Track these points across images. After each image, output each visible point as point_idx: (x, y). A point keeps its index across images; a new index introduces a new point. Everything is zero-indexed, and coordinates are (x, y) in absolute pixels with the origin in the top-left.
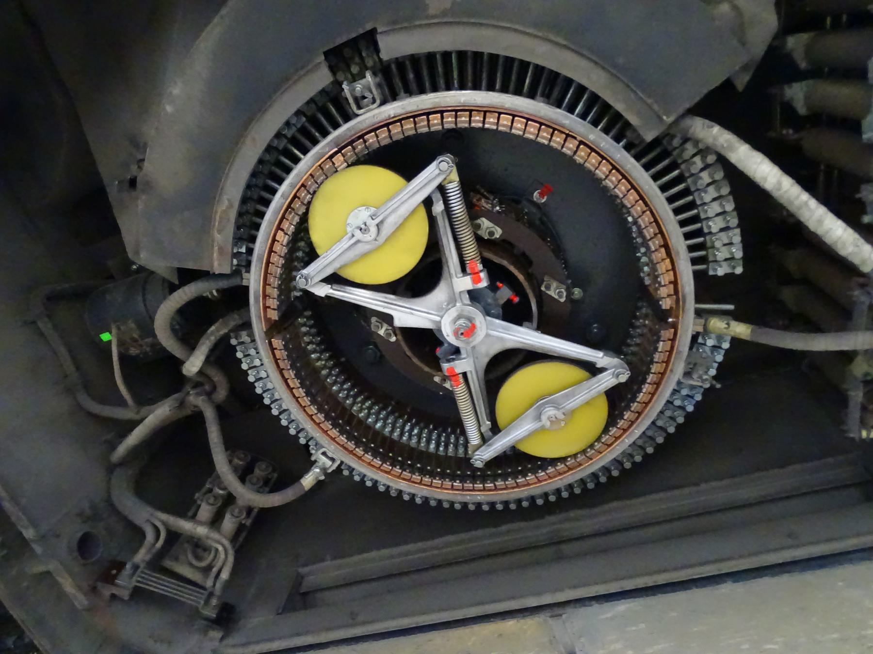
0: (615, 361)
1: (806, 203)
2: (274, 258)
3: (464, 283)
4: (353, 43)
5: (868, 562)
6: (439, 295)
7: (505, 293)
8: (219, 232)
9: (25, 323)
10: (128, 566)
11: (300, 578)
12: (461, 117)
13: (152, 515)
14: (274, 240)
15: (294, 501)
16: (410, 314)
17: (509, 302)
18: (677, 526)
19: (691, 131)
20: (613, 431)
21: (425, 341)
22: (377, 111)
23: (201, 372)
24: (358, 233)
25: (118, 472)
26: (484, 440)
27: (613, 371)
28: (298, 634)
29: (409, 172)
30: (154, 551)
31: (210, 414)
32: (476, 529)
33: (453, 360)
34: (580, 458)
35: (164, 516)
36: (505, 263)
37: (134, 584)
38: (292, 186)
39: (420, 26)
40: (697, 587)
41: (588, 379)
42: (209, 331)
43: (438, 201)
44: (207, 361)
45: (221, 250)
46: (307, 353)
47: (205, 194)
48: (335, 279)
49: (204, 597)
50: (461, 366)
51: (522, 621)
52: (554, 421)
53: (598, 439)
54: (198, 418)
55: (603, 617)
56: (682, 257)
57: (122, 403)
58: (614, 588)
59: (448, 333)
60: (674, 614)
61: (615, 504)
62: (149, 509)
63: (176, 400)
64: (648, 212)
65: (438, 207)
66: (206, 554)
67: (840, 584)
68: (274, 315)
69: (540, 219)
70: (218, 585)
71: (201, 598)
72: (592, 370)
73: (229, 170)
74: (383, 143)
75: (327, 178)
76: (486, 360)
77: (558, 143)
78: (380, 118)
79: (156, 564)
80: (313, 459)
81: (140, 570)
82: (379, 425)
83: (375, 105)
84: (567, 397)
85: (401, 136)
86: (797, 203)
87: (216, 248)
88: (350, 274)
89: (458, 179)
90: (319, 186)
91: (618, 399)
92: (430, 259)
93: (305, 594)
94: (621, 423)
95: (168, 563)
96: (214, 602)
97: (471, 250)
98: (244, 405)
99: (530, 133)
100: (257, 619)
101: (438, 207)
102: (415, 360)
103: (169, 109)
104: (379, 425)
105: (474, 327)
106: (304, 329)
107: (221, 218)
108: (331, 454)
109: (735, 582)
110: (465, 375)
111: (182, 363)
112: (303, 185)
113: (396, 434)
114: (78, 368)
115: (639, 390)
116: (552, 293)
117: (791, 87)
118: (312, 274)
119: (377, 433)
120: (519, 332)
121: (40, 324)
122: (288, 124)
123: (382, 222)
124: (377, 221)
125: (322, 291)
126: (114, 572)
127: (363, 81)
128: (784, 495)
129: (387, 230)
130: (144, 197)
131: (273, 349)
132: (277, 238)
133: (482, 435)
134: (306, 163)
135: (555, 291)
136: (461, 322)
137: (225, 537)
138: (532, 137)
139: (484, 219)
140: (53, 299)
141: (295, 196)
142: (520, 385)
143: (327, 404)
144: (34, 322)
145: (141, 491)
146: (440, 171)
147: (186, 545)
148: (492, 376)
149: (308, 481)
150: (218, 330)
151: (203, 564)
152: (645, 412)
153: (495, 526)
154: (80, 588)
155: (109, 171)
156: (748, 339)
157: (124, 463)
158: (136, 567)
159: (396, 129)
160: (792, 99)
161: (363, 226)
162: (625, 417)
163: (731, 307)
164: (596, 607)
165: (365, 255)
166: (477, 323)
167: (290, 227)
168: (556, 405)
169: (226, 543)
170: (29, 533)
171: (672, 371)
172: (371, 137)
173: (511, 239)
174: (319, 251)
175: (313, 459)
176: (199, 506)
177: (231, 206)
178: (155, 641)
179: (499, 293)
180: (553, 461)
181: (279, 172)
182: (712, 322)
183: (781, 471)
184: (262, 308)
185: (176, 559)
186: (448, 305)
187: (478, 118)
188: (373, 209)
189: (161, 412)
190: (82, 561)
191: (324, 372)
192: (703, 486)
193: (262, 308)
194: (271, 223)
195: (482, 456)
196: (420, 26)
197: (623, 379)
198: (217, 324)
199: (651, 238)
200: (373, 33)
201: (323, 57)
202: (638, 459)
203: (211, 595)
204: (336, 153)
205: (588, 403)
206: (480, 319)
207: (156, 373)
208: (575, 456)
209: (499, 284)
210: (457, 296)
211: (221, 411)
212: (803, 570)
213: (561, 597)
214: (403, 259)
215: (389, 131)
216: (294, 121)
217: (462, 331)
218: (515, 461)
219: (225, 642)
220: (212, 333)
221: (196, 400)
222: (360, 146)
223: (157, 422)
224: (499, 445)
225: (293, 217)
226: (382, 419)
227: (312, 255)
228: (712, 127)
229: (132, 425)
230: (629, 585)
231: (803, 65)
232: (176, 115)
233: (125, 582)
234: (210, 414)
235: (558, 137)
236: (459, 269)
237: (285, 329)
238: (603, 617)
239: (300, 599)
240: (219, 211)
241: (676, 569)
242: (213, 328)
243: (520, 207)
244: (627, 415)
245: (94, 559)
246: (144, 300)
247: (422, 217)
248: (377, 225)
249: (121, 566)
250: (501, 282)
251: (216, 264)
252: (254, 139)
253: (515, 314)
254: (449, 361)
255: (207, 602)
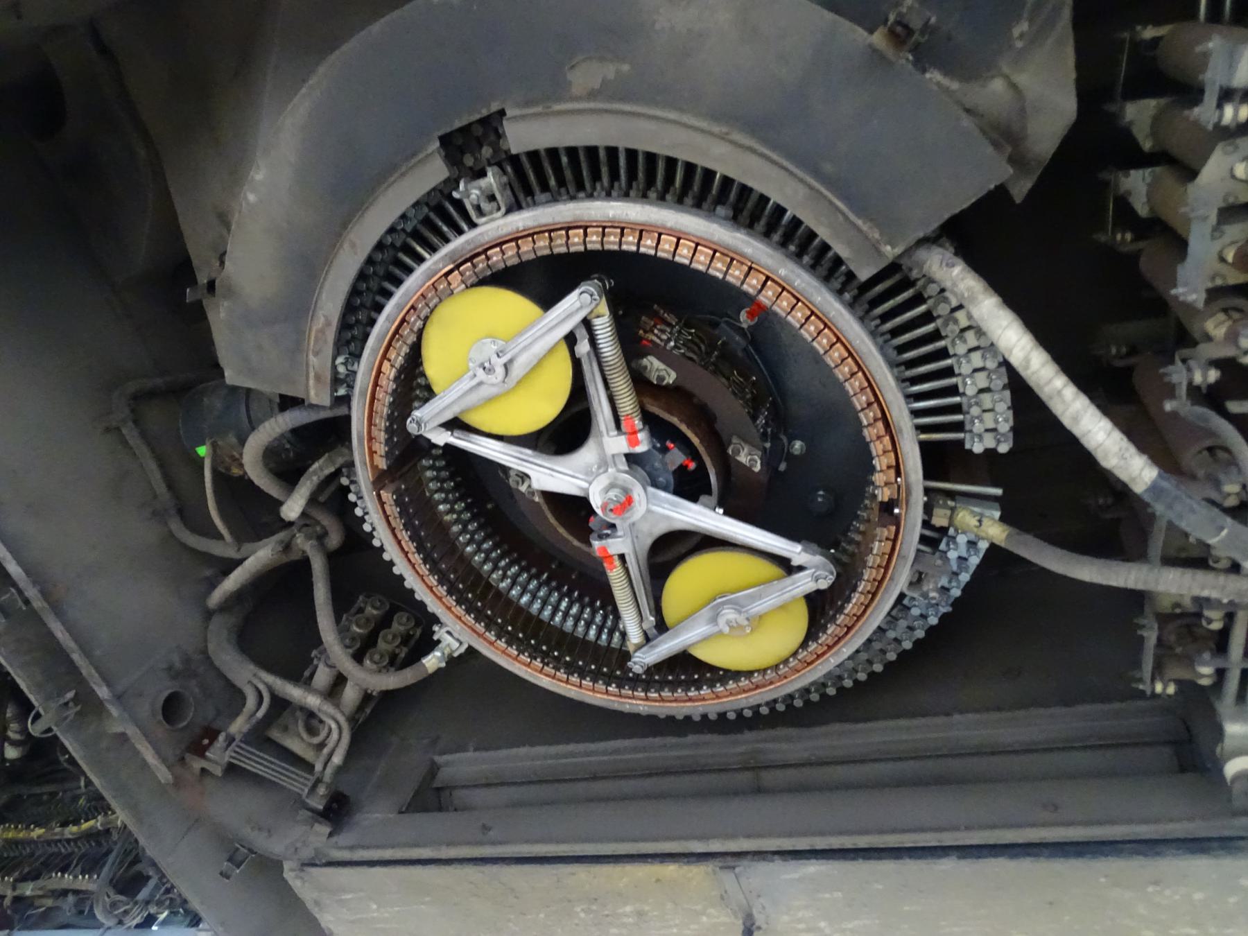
0: (818, 559)
1: (1059, 392)
2: (380, 394)
3: (617, 444)
4: (484, 121)
5: (1141, 857)
6: (586, 455)
7: (677, 457)
8: (316, 354)
9: (108, 430)
10: (221, 738)
11: (434, 769)
12: (610, 234)
13: (255, 675)
14: (379, 372)
15: (413, 685)
16: (550, 475)
17: (682, 469)
18: (909, 767)
19: (926, 267)
20: (813, 646)
21: (574, 510)
22: (501, 222)
23: (304, 514)
24: (480, 372)
25: (217, 621)
26: (647, 639)
27: (815, 571)
28: (417, 845)
29: (547, 301)
30: (254, 721)
31: (318, 566)
32: (655, 736)
33: (608, 536)
34: (770, 675)
35: (270, 679)
36: (675, 420)
37: (227, 759)
38: (399, 307)
39: (560, 113)
40: (910, 857)
41: (778, 579)
42: (311, 469)
43: (583, 338)
44: (313, 500)
45: (318, 378)
46: (431, 505)
47: (297, 308)
48: (455, 424)
49: (310, 784)
50: (616, 546)
51: (686, 868)
52: (735, 627)
53: (795, 654)
54: (305, 563)
55: (788, 877)
56: (905, 436)
57: (219, 537)
58: (802, 844)
59: (596, 502)
60: (880, 887)
61: (837, 727)
62: (252, 667)
63: (281, 542)
64: (860, 374)
65: (583, 347)
66: (321, 726)
67: (1103, 880)
68: (382, 464)
69: (745, 350)
70: (329, 771)
71: (305, 785)
72: (787, 566)
73: (325, 279)
74: (509, 263)
75: (441, 301)
76: (649, 542)
77: (737, 278)
78: (505, 231)
79: (259, 737)
80: (435, 638)
81: (234, 744)
82: (525, 599)
83: (499, 214)
84: (753, 598)
85: (532, 256)
86: (1047, 389)
87: (312, 375)
88: (473, 419)
89: (608, 313)
90: (432, 312)
91: (820, 607)
92: (575, 409)
93: (438, 789)
94: (823, 638)
95: (275, 734)
96: (322, 790)
97: (627, 404)
98: (356, 563)
99: (699, 262)
100: (375, 815)
101: (583, 347)
102: (561, 530)
103: (252, 197)
104: (525, 599)
105: (629, 501)
106: (429, 474)
107: (316, 337)
108: (456, 633)
109: (959, 858)
110: (622, 557)
111: (281, 503)
112: (413, 307)
113: (547, 613)
114: (170, 487)
115: (848, 600)
116: (743, 458)
117: (1127, 176)
118: (426, 418)
119: (520, 611)
120: (690, 510)
121: (124, 431)
122: (404, 217)
123: (511, 361)
124: (505, 359)
125: (441, 438)
126: (206, 741)
127: (483, 182)
128: (1060, 746)
129: (518, 370)
130: (226, 304)
131: (382, 504)
132: (383, 369)
133: (645, 634)
134: (413, 283)
135: (748, 457)
136: (612, 494)
137: (343, 713)
138: (701, 268)
139: (651, 358)
140: (139, 398)
141: (403, 321)
142: (690, 580)
143: (455, 572)
144: (118, 429)
145: (245, 643)
146: (583, 302)
147: (298, 713)
148: (660, 559)
149: (432, 662)
150: (321, 469)
151: (316, 740)
152: (856, 628)
153: (679, 736)
154: (164, 760)
155: (198, 251)
156: (1003, 545)
157: (225, 607)
158: (230, 740)
159: (526, 246)
160: (1129, 193)
161: (487, 365)
162: (829, 632)
163: (998, 492)
164: (777, 865)
165: (490, 400)
166: (635, 497)
167: (398, 356)
168: (738, 606)
169: (342, 719)
170: (103, 692)
171: (891, 579)
172: (496, 254)
173: (688, 386)
174: (435, 389)
175: (435, 638)
176: (316, 667)
177: (328, 324)
178: (252, 828)
179: (669, 457)
180: (736, 675)
181: (397, 272)
182: (961, 515)
183: (1064, 710)
184: (367, 451)
185: (285, 729)
186: (599, 468)
187: (631, 239)
188: (501, 343)
189: (261, 556)
190: (167, 726)
191: (455, 529)
192: (957, 717)
193: (367, 451)
194: (375, 351)
195: (643, 659)
196: (560, 113)
197: (824, 585)
198: (321, 461)
199: (863, 409)
200: (502, 113)
201: (438, 144)
202: (862, 676)
203: (319, 781)
204: (451, 272)
205: (783, 607)
206: (638, 492)
207: (252, 512)
208: (763, 671)
209: (669, 444)
210: (610, 460)
211: (333, 558)
212: (1052, 856)
213: (733, 846)
214: (543, 405)
215: (518, 247)
216: (412, 213)
217: (612, 506)
218: (685, 669)
219: (335, 839)
220: (315, 473)
221: (304, 544)
222: (481, 263)
223: (259, 567)
224: (666, 647)
225: (401, 347)
226: (531, 592)
227: (429, 393)
228: (953, 266)
229: (228, 566)
230: (820, 843)
231: (1147, 145)
232: (266, 203)
233: (218, 755)
234: (318, 566)
235: (737, 268)
236: (612, 424)
237: (401, 476)
238: (788, 877)
239: (431, 797)
240: (314, 329)
241: (882, 832)
242: (316, 465)
243: (717, 332)
244: (831, 629)
245: (185, 723)
246: (248, 410)
247: (564, 351)
248: (505, 365)
249: (212, 734)
250: (673, 442)
251: (312, 393)
252: (353, 246)
253: (689, 486)
254: (601, 537)
255: (314, 788)
